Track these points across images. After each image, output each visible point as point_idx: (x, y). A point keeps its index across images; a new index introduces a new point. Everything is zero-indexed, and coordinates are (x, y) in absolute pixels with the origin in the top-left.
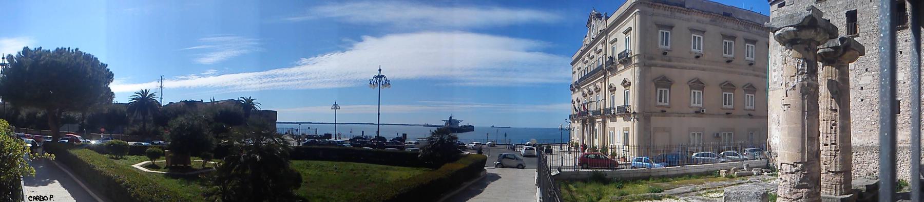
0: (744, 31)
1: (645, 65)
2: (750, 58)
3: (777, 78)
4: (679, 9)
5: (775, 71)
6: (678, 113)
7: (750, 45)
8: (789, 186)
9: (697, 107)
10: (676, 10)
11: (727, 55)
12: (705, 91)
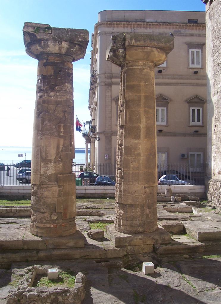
1: (105, 85)
4: (138, 25)
12: (169, 107)
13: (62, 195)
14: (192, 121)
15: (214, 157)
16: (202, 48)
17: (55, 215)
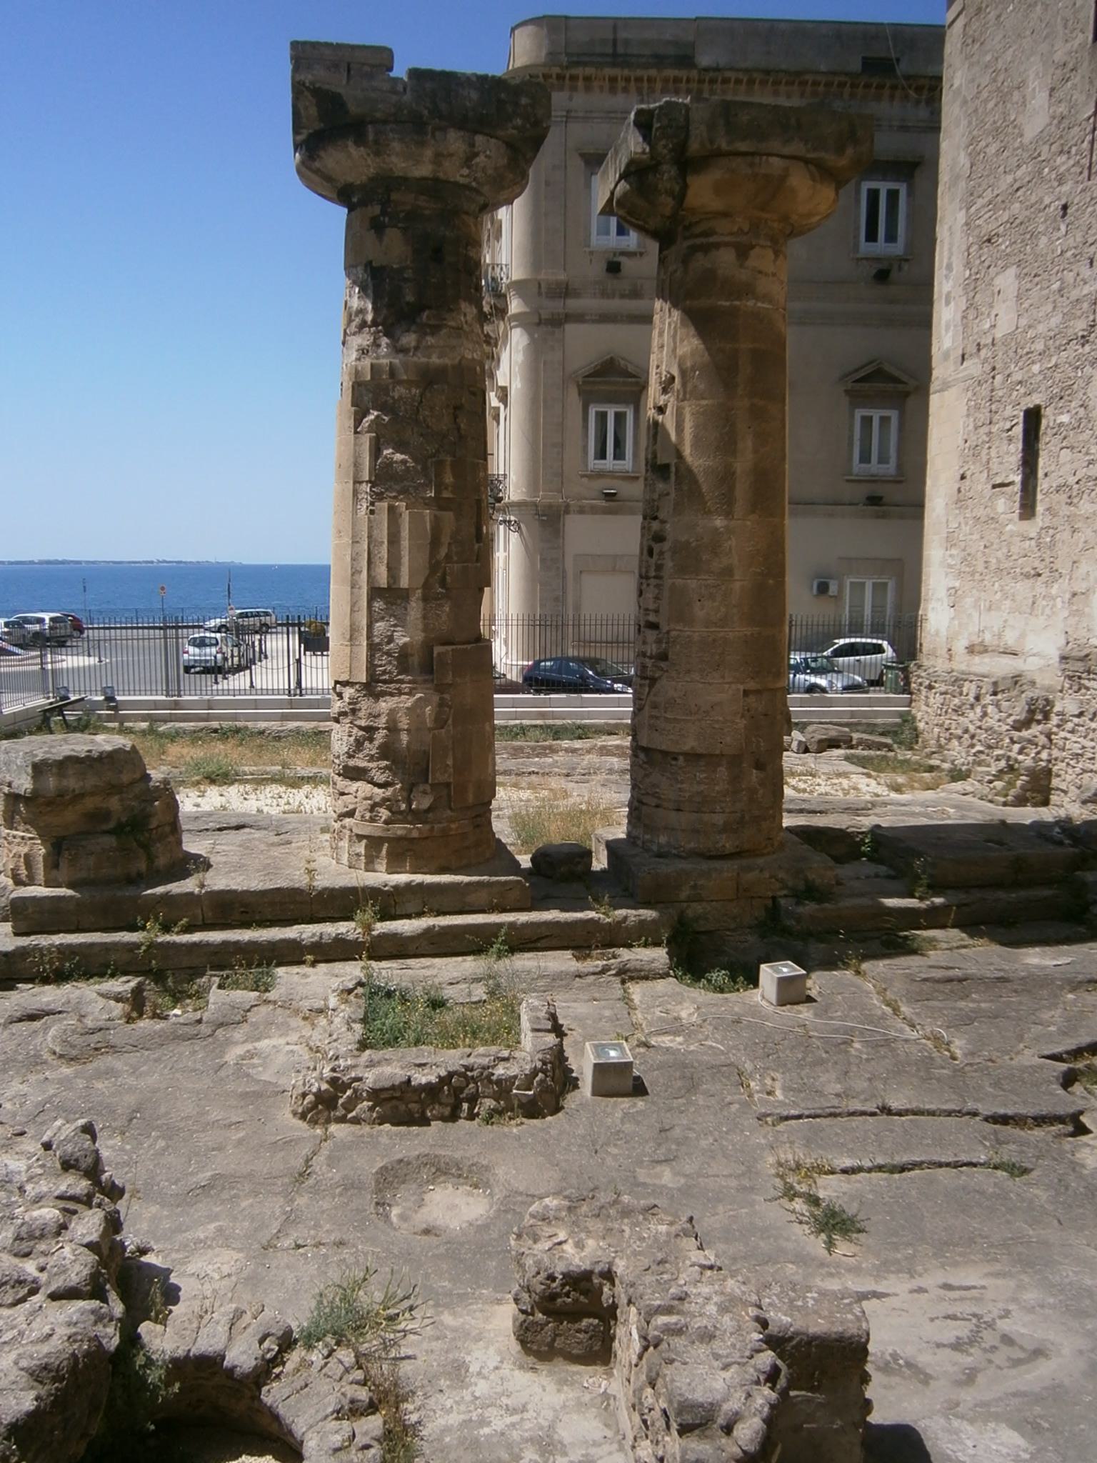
13: (450, 722)
14: (596, 458)
15: (953, 591)
17: (425, 792)
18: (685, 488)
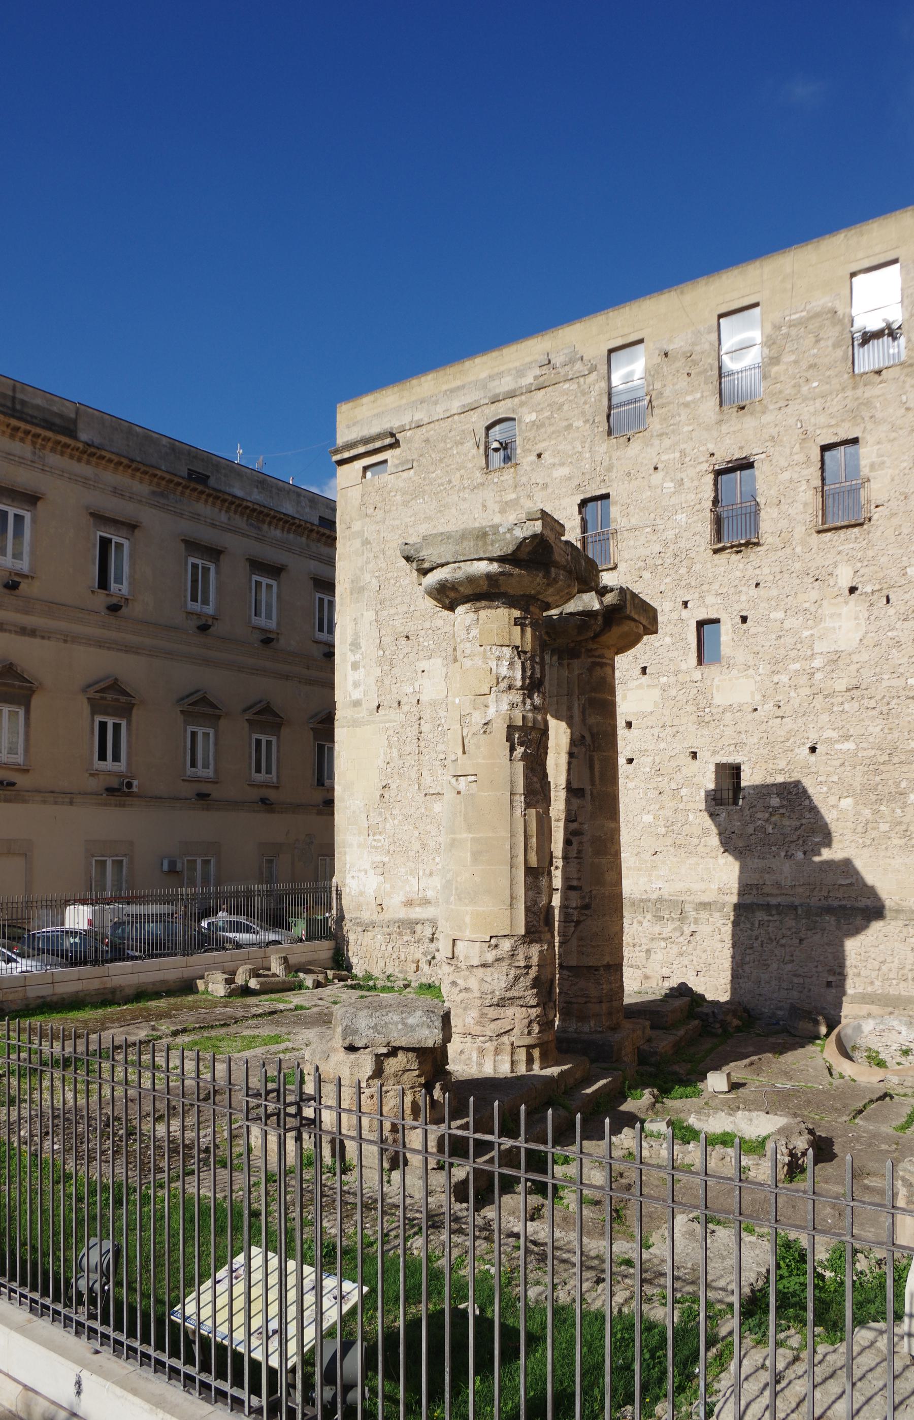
0: (248, 536)
2: (262, 621)
3: (361, 689)
5: (355, 666)
6: (52, 792)
7: (265, 581)
8: (478, 1002)
9: (110, 773)
10: (50, 444)
11: (197, 607)
12: (134, 718)
14: (99, 760)
16: (218, 560)
18: (597, 804)
